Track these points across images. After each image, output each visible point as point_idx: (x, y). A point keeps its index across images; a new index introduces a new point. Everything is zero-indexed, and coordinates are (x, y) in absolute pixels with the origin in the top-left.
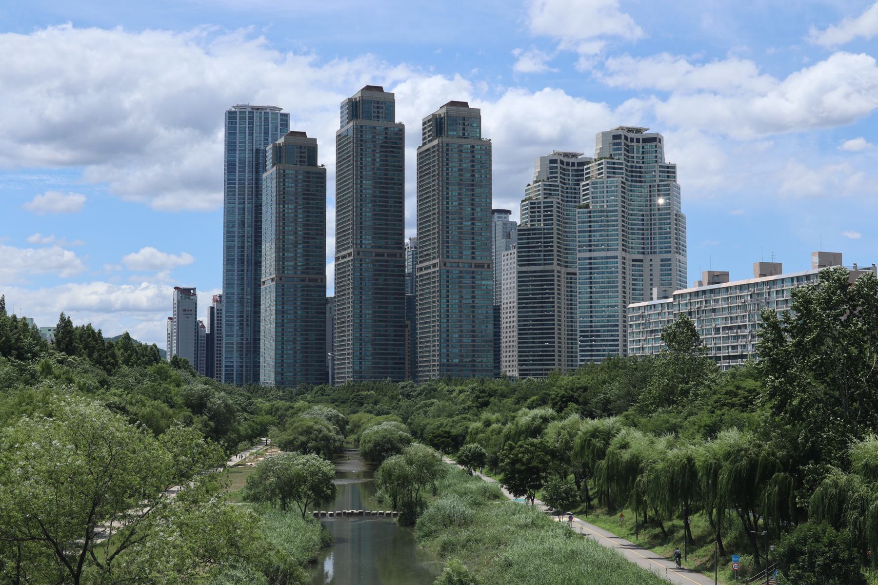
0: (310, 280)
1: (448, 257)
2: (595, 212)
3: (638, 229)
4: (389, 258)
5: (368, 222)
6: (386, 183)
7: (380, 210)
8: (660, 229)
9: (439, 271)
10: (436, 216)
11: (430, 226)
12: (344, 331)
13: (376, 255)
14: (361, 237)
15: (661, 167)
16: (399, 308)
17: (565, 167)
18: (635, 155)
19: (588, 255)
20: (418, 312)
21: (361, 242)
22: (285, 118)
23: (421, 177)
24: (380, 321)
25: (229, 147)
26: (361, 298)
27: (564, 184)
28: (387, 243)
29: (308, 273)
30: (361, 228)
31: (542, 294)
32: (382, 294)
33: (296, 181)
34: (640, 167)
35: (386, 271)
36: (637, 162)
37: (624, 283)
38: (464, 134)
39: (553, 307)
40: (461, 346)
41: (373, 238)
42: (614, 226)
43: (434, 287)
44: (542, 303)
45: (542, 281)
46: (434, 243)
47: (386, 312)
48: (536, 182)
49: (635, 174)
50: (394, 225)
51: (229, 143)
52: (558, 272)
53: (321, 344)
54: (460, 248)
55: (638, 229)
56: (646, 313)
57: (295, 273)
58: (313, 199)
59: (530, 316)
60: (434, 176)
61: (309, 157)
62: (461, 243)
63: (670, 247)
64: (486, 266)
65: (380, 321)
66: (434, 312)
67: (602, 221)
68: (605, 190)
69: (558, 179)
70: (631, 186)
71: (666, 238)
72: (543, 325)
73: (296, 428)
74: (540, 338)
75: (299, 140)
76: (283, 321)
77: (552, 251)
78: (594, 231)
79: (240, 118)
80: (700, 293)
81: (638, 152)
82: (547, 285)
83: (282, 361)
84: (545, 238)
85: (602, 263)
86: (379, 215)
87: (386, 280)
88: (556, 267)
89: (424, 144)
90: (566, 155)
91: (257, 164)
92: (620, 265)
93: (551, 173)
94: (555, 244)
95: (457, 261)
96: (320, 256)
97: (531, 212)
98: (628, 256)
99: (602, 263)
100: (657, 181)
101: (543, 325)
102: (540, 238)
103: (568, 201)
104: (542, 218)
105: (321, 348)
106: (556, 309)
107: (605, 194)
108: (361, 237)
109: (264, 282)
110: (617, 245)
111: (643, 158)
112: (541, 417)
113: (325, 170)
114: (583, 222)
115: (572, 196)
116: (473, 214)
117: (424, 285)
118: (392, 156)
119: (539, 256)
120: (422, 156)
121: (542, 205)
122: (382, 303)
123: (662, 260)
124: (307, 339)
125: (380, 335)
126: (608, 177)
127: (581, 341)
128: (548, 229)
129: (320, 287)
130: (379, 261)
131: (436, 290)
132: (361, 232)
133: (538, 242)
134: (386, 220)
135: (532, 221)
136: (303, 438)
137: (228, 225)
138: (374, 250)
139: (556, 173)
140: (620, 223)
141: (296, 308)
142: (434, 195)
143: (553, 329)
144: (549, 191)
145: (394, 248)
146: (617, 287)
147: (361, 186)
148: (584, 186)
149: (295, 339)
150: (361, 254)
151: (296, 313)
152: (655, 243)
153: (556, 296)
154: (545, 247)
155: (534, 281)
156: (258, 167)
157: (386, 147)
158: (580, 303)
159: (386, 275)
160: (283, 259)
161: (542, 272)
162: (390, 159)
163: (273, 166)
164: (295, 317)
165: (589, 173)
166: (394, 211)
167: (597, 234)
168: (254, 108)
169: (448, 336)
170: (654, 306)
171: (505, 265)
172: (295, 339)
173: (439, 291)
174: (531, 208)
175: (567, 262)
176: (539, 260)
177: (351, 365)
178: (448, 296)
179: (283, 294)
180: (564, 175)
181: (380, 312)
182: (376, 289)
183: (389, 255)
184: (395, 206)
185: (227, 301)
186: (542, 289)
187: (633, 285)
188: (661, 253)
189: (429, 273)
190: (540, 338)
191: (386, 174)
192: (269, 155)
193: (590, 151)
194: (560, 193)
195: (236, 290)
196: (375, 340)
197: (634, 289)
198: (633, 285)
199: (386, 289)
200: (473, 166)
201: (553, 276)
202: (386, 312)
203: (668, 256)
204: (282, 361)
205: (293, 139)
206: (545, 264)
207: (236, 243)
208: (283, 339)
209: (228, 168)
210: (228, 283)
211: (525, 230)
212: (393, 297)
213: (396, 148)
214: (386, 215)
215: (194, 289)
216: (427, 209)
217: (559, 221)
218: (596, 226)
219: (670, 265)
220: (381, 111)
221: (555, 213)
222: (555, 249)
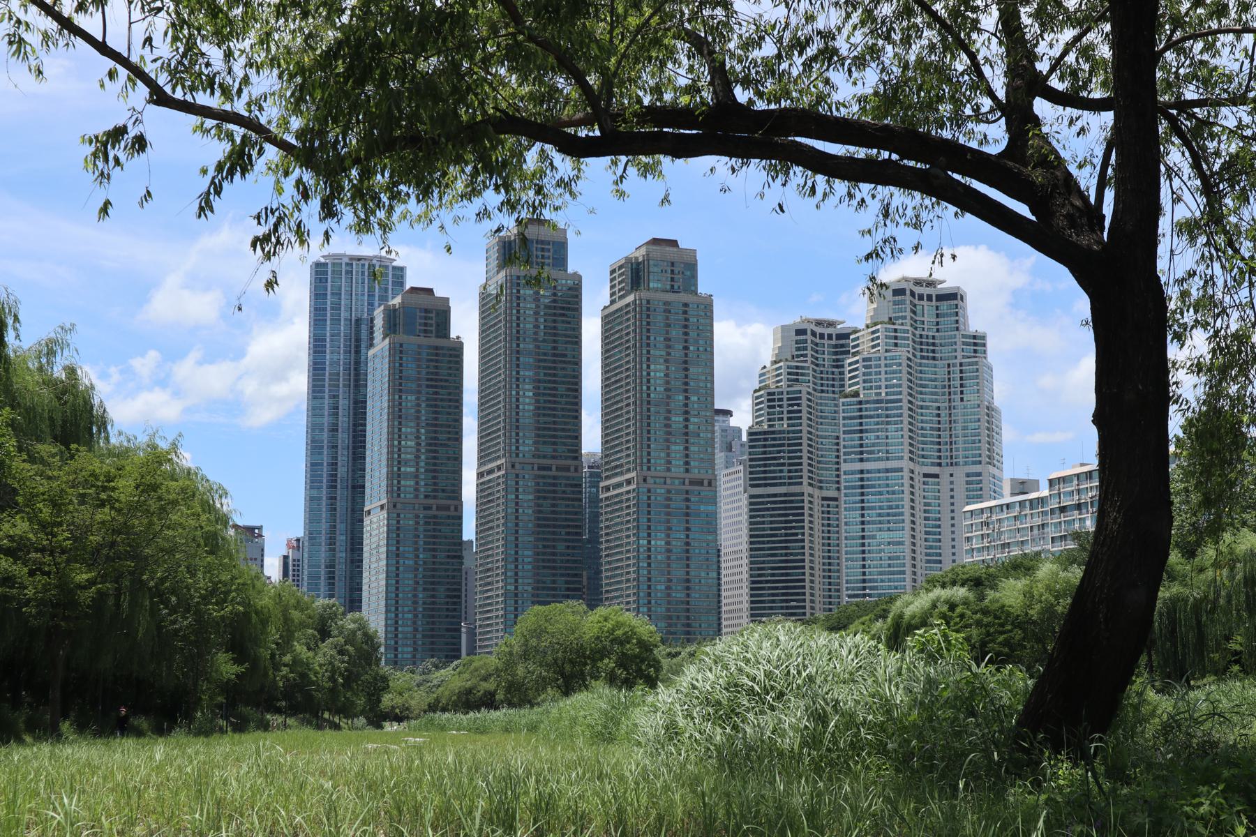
0: (439, 508)
1: (649, 469)
2: (867, 402)
3: (932, 429)
4: (560, 474)
5: (527, 418)
6: (554, 362)
7: (545, 402)
8: (964, 428)
10: (632, 407)
11: (621, 423)
12: (489, 584)
13: (539, 469)
14: (517, 441)
17: (818, 341)
18: (925, 319)
19: (858, 466)
20: (603, 554)
21: (517, 448)
23: (607, 351)
24: (544, 567)
26: (517, 532)
27: (817, 365)
28: (555, 451)
29: (435, 497)
30: (517, 427)
31: (785, 528)
32: (548, 526)
34: (934, 337)
35: (554, 492)
37: (913, 508)
38: (672, 286)
39: (803, 547)
40: (669, 603)
41: (535, 443)
42: (896, 423)
43: (628, 514)
44: (786, 541)
45: (785, 509)
46: (628, 448)
48: (775, 362)
51: (316, 309)
52: (810, 495)
53: (455, 603)
55: (932, 429)
56: (994, 518)
58: (442, 387)
59: (769, 562)
60: (628, 348)
61: (438, 325)
63: (980, 455)
64: (706, 482)
65: (544, 567)
66: (628, 551)
67: (878, 416)
70: (920, 365)
72: (787, 575)
74: (783, 594)
75: (422, 300)
76: (398, 569)
77: (801, 464)
78: (867, 431)
79: (333, 272)
82: (793, 515)
84: (789, 445)
85: (879, 479)
86: (544, 408)
87: (553, 505)
88: (807, 489)
89: (612, 302)
90: (819, 323)
91: (358, 340)
92: (907, 482)
93: (798, 349)
94: (805, 455)
97: (769, 407)
98: (917, 469)
99: (879, 479)
101: (787, 575)
102: (783, 445)
103: (822, 391)
104: (785, 416)
105: (455, 610)
106: (807, 551)
108: (517, 441)
109: (369, 512)
110: (902, 450)
111: (938, 323)
112: (947, 602)
114: (851, 418)
115: (833, 380)
116: (686, 405)
117: (612, 512)
118: (563, 322)
119: (781, 471)
120: (609, 321)
121: (785, 396)
123: (968, 475)
124: (433, 596)
125: (543, 589)
126: (887, 351)
128: (794, 432)
129: (453, 518)
130: (544, 477)
132: (517, 434)
133: (779, 452)
134: (554, 416)
135: (769, 420)
137: (313, 430)
138: (536, 461)
139: (805, 349)
140: (906, 419)
141: (417, 549)
142: (628, 377)
143: (804, 581)
144: (795, 375)
145: (566, 458)
148: (850, 364)
149: (415, 596)
150: (517, 466)
152: (957, 450)
153: (807, 531)
154: (790, 458)
155: (773, 509)
156: (358, 342)
157: (555, 308)
158: (846, 538)
159: (554, 499)
160: (399, 476)
161: (785, 495)
162: (559, 325)
163: (384, 339)
164: (416, 563)
165: (857, 346)
166: (567, 403)
167: (872, 435)
168: (352, 258)
169: (649, 587)
170: (1008, 506)
171: (726, 489)
172: (415, 596)
173: (637, 520)
175: (821, 482)
176: (781, 478)
178: (649, 528)
179: (398, 529)
180: (817, 352)
181: (544, 554)
182: (539, 519)
183: (558, 469)
184: (568, 396)
186: (786, 522)
187: (925, 511)
188: (966, 463)
189: (621, 494)
190: (783, 594)
191: (555, 348)
192: (379, 322)
194: (811, 378)
195: (324, 527)
196: (538, 596)
197: (926, 519)
198: (925, 511)
200: (686, 334)
201: (803, 501)
203: (977, 469)
204: (396, 629)
206: (790, 484)
207: (325, 458)
208: (397, 595)
209: (315, 346)
210: (312, 517)
211: (760, 433)
212: (563, 531)
213: (569, 309)
215: (260, 528)
216: (617, 399)
217: (810, 419)
220: (546, 254)
221: (804, 409)
222: (805, 461)
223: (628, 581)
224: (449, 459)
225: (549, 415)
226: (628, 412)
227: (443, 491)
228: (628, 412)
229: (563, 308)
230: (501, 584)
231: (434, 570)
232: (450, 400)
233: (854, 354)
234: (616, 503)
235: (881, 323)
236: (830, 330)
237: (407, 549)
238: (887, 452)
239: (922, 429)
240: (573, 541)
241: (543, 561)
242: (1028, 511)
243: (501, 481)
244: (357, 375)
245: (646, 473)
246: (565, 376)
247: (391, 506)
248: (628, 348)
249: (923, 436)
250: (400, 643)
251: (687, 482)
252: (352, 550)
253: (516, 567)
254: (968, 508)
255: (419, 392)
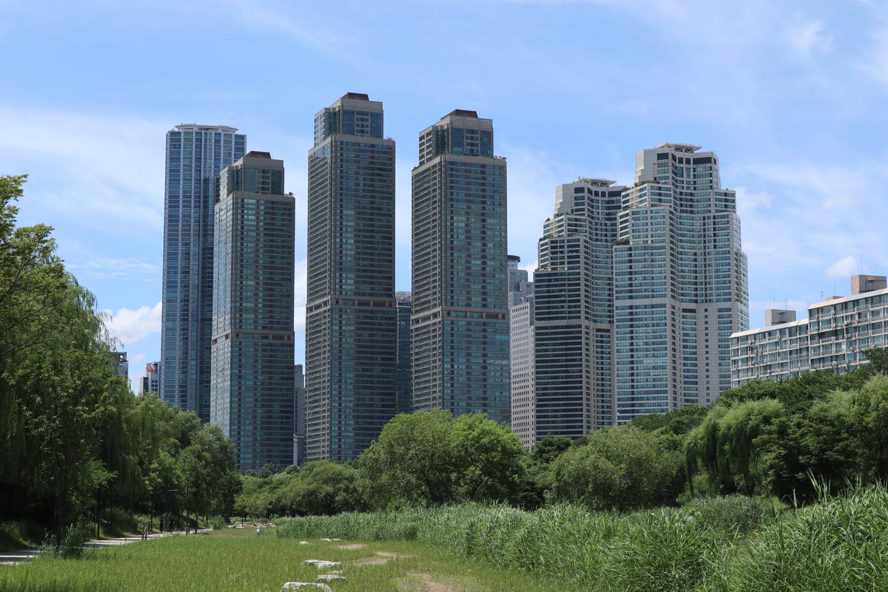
0: (274, 337)
1: (452, 304)
2: (636, 249)
3: (689, 271)
4: (376, 308)
8: (717, 271)
9: (442, 322)
12: (316, 401)
14: (341, 281)
15: (716, 194)
16: (388, 371)
18: (685, 179)
19: (628, 303)
21: (341, 287)
22: (241, 140)
24: (364, 387)
25: (171, 176)
26: (340, 357)
28: (372, 289)
29: (271, 328)
33: (258, 213)
34: (691, 194)
35: (372, 324)
36: (688, 188)
37: (674, 338)
39: (581, 371)
43: (434, 343)
44: (566, 366)
46: (434, 287)
47: (371, 376)
48: (558, 215)
49: (686, 203)
50: (381, 266)
51: (171, 171)
52: (587, 327)
53: (288, 418)
54: (468, 293)
55: (689, 271)
56: (758, 344)
57: (256, 328)
60: (435, 202)
61: (274, 184)
62: (468, 286)
63: (730, 294)
64: (500, 316)
65: (364, 387)
66: (435, 374)
68: (649, 221)
69: (586, 212)
71: (725, 283)
72: (567, 394)
73: (317, 474)
75: (261, 162)
76: (240, 388)
80: (850, 305)
81: (689, 176)
83: (239, 439)
84: (569, 285)
86: (364, 253)
87: (371, 335)
88: (583, 322)
89: (421, 164)
92: (669, 316)
95: (464, 309)
96: (287, 307)
97: (552, 253)
98: (678, 305)
100: (713, 211)
101: (567, 394)
102: (564, 285)
103: (597, 240)
104: (566, 260)
106: (584, 374)
107: (649, 227)
109: (216, 341)
111: (695, 183)
113: (294, 199)
115: (607, 231)
116: (484, 251)
118: (380, 180)
119: (562, 307)
120: (419, 180)
121: (566, 244)
122: (367, 364)
123: (720, 310)
125: (363, 405)
127: (620, 412)
129: (287, 345)
130: (363, 311)
131: (437, 346)
132: (341, 275)
133: (561, 291)
134: (372, 260)
135: (552, 264)
136: (329, 489)
137: (168, 273)
138: (357, 297)
139: (583, 204)
142: (434, 227)
143: (581, 399)
144: (574, 227)
145: (382, 295)
146: (665, 343)
147: (341, 217)
148: (621, 217)
149: (255, 411)
150: (341, 302)
151: (256, 378)
152: (711, 289)
156: (206, 199)
157: (372, 169)
159: (372, 329)
161: (566, 327)
163: (228, 195)
164: (255, 383)
165: (627, 201)
167: (640, 277)
172: (255, 411)
173: (443, 347)
174: (552, 248)
176: (562, 312)
177: (327, 443)
178: (452, 354)
179: (240, 355)
181: (364, 376)
182: (359, 346)
183: (375, 304)
185: (167, 368)
187: (684, 341)
188: (718, 300)
189: (429, 325)
191: (372, 203)
193: (625, 177)
194: (587, 229)
195: (178, 354)
196: (358, 411)
197: (685, 347)
198: (684, 341)
199: (372, 347)
202: (371, 376)
204: (239, 439)
205: (254, 160)
206: (570, 318)
207: (179, 295)
208: (239, 411)
211: (545, 275)
212: (379, 357)
213: (384, 170)
214: (372, 254)
218: (637, 267)
219: (730, 316)
220: (365, 123)
223: (434, 398)
224: (283, 296)
225: (367, 259)
226: (434, 257)
227: (278, 323)
228: (434, 257)
229: (379, 169)
230: (327, 401)
231: (270, 389)
232: (284, 247)
233: (625, 208)
234: (424, 333)
235: (648, 182)
236: (603, 189)
237: (248, 372)
238: (653, 291)
239: (682, 271)
240: (388, 365)
241: (363, 382)
242: (787, 338)
243: (327, 314)
244: (205, 226)
245: (449, 308)
246: (381, 226)
247: (234, 335)
248: (435, 202)
249: (683, 277)
250: (242, 450)
251: (484, 315)
252: (201, 373)
253: (340, 387)
254: (734, 335)
255: (258, 240)
